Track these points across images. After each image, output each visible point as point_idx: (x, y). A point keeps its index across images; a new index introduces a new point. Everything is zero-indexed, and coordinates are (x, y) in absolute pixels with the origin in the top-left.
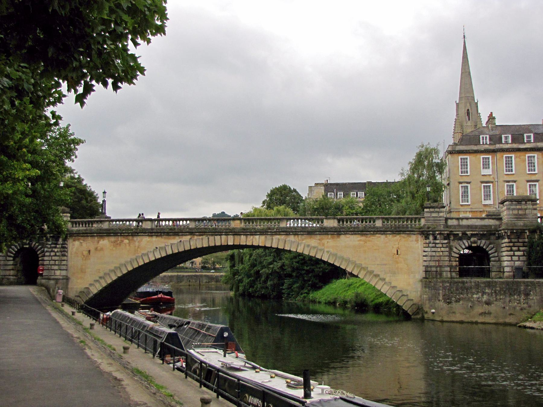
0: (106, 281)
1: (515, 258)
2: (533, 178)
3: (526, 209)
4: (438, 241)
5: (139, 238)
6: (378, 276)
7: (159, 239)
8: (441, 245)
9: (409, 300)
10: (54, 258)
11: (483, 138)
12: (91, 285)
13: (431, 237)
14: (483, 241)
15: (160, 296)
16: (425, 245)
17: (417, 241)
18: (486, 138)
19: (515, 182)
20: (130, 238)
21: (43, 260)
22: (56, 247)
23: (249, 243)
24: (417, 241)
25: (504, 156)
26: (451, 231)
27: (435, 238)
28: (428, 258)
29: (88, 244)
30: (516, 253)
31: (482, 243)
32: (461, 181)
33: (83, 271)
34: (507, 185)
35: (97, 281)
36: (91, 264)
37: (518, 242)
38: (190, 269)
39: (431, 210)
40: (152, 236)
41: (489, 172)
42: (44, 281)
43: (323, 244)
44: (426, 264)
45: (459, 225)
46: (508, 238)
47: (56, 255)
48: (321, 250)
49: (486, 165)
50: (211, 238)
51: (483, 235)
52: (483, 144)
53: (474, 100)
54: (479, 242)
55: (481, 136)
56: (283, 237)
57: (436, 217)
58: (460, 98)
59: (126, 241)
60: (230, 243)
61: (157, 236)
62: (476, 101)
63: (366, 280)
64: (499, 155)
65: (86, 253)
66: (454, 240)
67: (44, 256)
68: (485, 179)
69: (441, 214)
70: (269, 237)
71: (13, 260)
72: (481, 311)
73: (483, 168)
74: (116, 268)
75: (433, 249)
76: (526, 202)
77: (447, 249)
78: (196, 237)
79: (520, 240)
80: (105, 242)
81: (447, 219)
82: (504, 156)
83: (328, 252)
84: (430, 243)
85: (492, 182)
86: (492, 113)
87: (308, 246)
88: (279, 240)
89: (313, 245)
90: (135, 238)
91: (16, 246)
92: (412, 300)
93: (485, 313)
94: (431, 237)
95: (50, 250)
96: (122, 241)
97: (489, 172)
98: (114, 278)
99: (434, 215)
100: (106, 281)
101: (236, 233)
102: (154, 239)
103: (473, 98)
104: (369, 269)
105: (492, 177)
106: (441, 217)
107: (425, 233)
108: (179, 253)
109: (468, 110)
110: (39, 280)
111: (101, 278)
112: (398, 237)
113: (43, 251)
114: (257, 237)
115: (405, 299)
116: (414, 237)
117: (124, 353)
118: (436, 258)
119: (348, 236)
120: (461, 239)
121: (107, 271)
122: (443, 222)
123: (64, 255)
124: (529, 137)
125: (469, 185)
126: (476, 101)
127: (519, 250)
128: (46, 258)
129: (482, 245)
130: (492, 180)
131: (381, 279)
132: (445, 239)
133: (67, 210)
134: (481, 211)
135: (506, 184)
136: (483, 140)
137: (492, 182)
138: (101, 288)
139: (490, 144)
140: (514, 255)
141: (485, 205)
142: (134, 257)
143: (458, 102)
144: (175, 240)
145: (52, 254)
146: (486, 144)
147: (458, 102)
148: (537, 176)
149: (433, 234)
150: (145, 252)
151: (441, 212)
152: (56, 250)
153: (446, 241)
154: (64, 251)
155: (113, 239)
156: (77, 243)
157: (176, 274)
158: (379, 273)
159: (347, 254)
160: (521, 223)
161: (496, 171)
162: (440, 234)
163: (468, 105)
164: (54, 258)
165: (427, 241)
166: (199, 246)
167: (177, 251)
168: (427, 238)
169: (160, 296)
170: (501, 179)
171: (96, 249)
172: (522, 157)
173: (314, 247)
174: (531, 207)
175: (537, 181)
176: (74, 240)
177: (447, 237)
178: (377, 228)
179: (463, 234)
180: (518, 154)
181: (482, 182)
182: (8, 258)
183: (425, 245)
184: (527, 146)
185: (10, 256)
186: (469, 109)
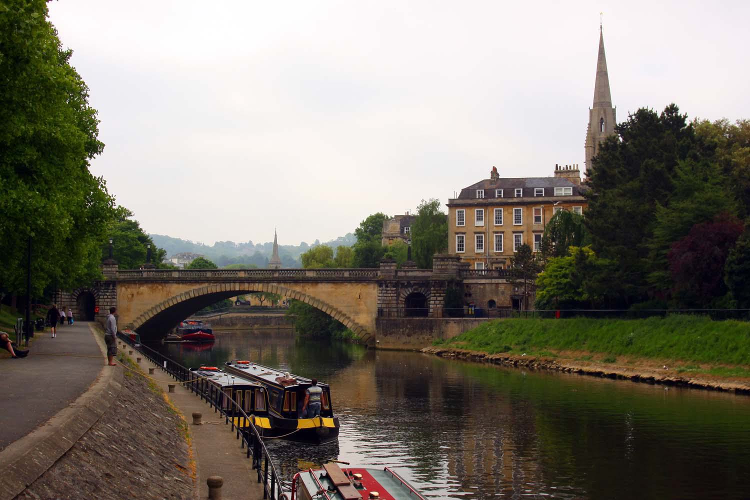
0: (145, 318)
1: (437, 302)
2: (519, 229)
3: (447, 265)
4: (389, 289)
5: (170, 285)
6: (345, 315)
7: (184, 286)
8: (390, 292)
9: (367, 333)
10: (107, 300)
11: (479, 192)
12: (134, 321)
13: (384, 286)
14: (423, 289)
15: (199, 333)
16: (379, 291)
17: (374, 288)
18: (482, 192)
19: (503, 232)
20: (163, 285)
21: (98, 302)
22: (107, 292)
23: (251, 289)
24: (374, 288)
25: (495, 209)
26: (398, 281)
27: (387, 286)
28: (381, 302)
29: (133, 289)
30: (439, 298)
31: (422, 290)
32: (458, 231)
33: (128, 310)
34: (496, 236)
35: (138, 318)
36: (138, 304)
37: (440, 290)
38: (284, 309)
39: (385, 264)
40: (179, 283)
41: (481, 223)
42: (99, 318)
43: (305, 291)
44: (380, 306)
45: (406, 276)
46: (434, 287)
47: (107, 298)
48: (303, 295)
49: (479, 218)
50: (223, 285)
51: (423, 284)
52: (479, 198)
53: (611, 106)
54: (420, 289)
55: (477, 191)
56: (275, 284)
57: (388, 270)
58: (595, 104)
59: (160, 287)
60: (237, 289)
61: (183, 283)
62: (613, 107)
63: (337, 318)
64: (490, 209)
65: (130, 296)
66: (401, 288)
67: (99, 298)
68: (478, 230)
69: (392, 268)
70: (266, 285)
71: (77, 301)
72: (405, 341)
73: (477, 219)
74: (152, 308)
75: (385, 295)
76: (448, 259)
77: (395, 295)
78: (212, 284)
79: (442, 288)
80: (144, 289)
81: (396, 272)
82: (495, 209)
83: (309, 296)
84: (383, 290)
85: (484, 233)
86: (495, 169)
87: (294, 291)
88: (273, 286)
89: (298, 291)
90: (167, 285)
91: (78, 291)
92: (370, 334)
93: (406, 342)
94: (384, 286)
95: (104, 294)
96: (157, 287)
97: (481, 223)
98: (152, 316)
99: (387, 268)
100: (145, 318)
101: (241, 281)
102: (181, 286)
103: (610, 104)
104: (339, 310)
105: (484, 228)
106: (392, 270)
107: (380, 283)
108: (186, 300)
109: (602, 119)
110: (96, 318)
111: (141, 316)
112: (360, 285)
113: (98, 295)
114: (257, 284)
115: (364, 333)
116: (372, 286)
117: (138, 362)
118: (387, 302)
119: (323, 284)
120: (407, 287)
121: (146, 311)
122: (393, 274)
123: (113, 298)
124: (518, 192)
125: (464, 235)
126: (613, 107)
127: (440, 296)
128: (100, 300)
129: (422, 292)
130: (484, 231)
131: (346, 318)
132: (394, 287)
133: (116, 262)
134: (473, 259)
135: (495, 235)
136: (479, 194)
137: (484, 233)
138: (141, 324)
139: (485, 198)
140: (437, 300)
141: (477, 254)
142: (166, 300)
143: (592, 108)
144: (196, 287)
145: (106, 297)
146: (482, 197)
147: (592, 108)
148: (522, 227)
149: (386, 283)
150: (174, 296)
151: (393, 266)
152: (108, 294)
153: (395, 289)
154: (114, 295)
155: (150, 285)
156: (123, 289)
157: (261, 315)
158: (346, 313)
159: (323, 298)
160: (443, 275)
161: (488, 222)
162: (390, 283)
163: (602, 112)
164: (107, 300)
165: (381, 288)
166: (214, 291)
167: (197, 295)
168: (380, 286)
169: (199, 333)
170: (491, 231)
171: (138, 293)
172: (510, 211)
173: (298, 293)
174: (451, 263)
175: (522, 232)
176: (121, 287)
177: (396, 285)
178: (345, 278)
179: (408, 283)
180: (506, 208)
181: (476, 233)
182: (73, 300)
183: (379, 291)
184: (515, 200)
185: (74, 298)
186: (603, 117)
